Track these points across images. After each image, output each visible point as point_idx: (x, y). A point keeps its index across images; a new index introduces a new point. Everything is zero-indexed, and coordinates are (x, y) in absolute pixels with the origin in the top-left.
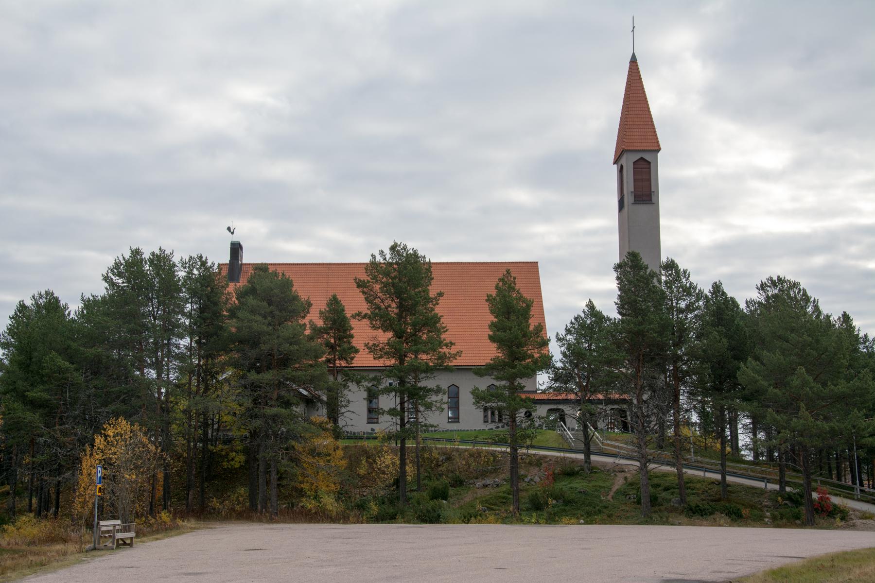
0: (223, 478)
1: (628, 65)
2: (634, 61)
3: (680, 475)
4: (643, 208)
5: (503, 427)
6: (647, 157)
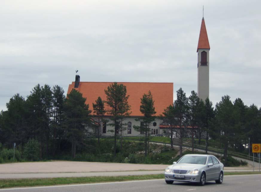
0: (62, 148)
1: (202, 21)
2: (203, 20)
3: (172, 147)
4: (204, 67)
5: (157, 136)
6: (206, 51)
